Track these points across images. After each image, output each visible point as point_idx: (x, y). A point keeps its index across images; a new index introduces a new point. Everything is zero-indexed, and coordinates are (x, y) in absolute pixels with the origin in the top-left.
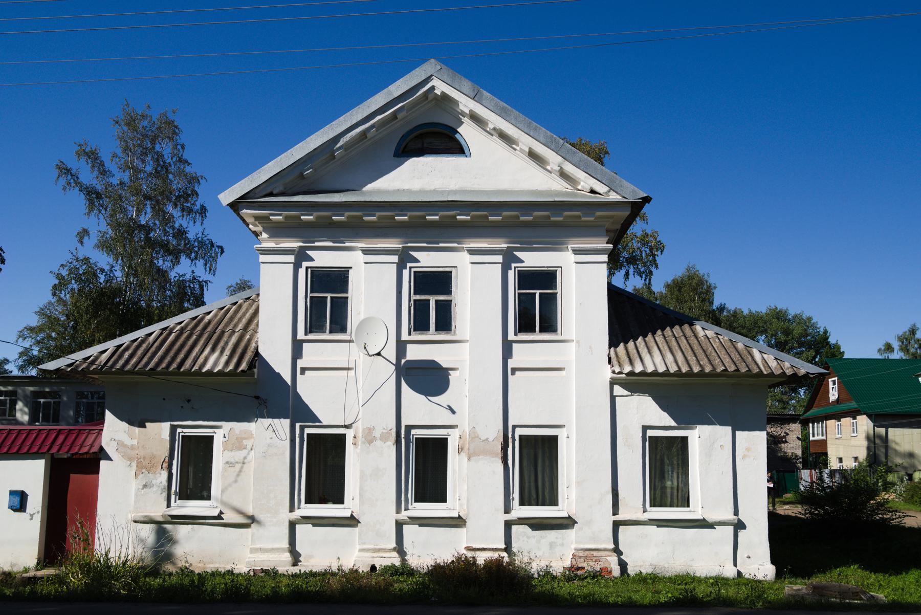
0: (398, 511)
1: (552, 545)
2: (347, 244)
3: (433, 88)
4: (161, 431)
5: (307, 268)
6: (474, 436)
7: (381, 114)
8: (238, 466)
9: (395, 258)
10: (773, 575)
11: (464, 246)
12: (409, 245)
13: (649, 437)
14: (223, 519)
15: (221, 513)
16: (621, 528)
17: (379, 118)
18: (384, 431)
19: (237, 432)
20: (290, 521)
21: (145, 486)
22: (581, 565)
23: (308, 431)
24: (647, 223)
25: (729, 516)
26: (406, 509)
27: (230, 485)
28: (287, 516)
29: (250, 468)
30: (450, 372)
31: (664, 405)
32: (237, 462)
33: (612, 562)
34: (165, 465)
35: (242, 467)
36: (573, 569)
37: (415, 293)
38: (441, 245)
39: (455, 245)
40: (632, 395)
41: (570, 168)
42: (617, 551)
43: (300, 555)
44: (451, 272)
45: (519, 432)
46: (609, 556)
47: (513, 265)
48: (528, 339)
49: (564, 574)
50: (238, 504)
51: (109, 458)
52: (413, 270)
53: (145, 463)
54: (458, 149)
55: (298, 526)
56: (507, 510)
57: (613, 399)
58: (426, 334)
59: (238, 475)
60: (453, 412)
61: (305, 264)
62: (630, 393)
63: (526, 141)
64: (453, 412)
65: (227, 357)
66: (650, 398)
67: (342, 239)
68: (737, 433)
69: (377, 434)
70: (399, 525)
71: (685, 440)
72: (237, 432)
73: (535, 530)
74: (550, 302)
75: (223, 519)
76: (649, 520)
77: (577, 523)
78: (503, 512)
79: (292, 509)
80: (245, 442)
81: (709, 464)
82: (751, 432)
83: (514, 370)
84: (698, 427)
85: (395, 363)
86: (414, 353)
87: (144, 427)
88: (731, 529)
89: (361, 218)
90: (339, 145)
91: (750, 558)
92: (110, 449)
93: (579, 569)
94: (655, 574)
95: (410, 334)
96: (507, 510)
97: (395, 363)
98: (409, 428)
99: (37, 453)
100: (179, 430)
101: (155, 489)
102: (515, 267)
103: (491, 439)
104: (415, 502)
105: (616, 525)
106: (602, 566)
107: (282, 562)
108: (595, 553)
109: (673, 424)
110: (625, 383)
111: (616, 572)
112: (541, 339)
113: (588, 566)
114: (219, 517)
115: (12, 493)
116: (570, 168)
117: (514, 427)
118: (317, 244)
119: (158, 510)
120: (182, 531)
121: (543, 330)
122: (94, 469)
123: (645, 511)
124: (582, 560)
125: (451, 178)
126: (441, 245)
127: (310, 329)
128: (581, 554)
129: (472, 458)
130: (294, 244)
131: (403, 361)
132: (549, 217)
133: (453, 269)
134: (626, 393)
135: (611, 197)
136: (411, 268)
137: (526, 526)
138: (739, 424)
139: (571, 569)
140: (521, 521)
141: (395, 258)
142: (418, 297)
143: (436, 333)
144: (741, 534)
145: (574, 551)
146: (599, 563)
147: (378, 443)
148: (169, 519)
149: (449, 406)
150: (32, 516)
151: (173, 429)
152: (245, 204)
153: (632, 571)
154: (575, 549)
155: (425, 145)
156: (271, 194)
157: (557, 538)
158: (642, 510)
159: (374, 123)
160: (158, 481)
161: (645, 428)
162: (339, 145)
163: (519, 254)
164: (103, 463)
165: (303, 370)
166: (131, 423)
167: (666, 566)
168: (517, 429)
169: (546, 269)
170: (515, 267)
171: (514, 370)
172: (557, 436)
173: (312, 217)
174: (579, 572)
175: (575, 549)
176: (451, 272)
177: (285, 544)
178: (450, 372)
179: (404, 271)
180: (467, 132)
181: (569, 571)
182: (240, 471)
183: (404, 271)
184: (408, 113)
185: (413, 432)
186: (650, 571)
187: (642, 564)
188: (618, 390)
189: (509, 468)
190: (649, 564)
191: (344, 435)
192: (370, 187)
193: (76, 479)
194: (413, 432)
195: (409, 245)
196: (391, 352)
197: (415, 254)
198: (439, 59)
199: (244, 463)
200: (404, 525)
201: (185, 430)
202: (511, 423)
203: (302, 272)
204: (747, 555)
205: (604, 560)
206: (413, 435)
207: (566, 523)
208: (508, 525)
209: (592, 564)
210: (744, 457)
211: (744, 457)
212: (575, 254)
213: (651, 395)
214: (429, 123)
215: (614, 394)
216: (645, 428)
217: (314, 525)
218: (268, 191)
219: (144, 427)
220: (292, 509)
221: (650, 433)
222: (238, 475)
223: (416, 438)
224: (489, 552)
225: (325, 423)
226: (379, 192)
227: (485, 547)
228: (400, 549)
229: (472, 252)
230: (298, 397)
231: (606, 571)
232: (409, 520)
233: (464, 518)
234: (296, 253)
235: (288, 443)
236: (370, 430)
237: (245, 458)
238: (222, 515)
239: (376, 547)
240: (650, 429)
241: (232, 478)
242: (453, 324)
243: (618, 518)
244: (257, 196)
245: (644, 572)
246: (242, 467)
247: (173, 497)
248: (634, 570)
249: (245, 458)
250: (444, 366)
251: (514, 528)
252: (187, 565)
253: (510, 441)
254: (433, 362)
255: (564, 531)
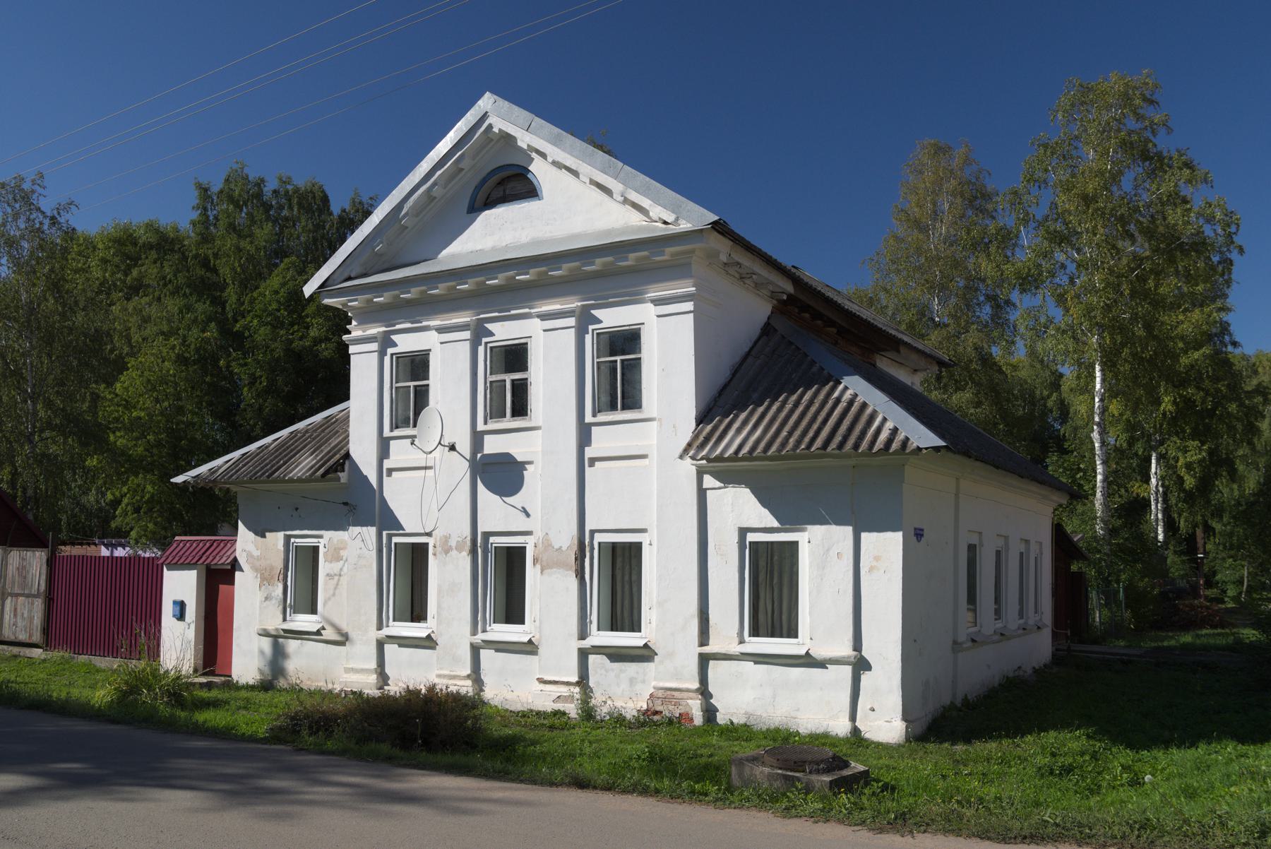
0: (474, 633)
1: (632, 681)
2: (424, 324)
3: (490, 126)
4: (276, 539)
5: (392, 355)
6: (547, 544)
7: (440, 169)
8: (336, 578)
9: (467, 335)
10: (901, 736)
11: (533, 311)
12: (482, 316)
13: (750, 543)
14: (322, 635)
15: (323, 628)
16: (712, 663)
17: (439, 173)
18: (459, 539)
19: (335, 541)
20: (377, 640)
21: (266, 598)
22: (659, 708)
23: (395, 540)
24: (1212, 187)
25: (846, 650)
26: (484, 631)
27: (329, 599)
28: (374, 634)
29: (344, 580)
30: (526, 466)
31: (765, 500)
32: (336, 575)
33: (695, 708)
34: (281, 577)
35: (339, 580)
36: (649, 713)
37: (491, 374)
38: (513, 312)
39: (526, 310)
40: (725, 487)
41: (634, 196)
42: (704, 692)
43: (388, 678)
44: (527, 344)
45: (599, 538)
46: (691, 699)
47: (591, 327)
48: (607, 420)
49: (637, 719)
50: (337, 620)
51: (242, 570)
52: (490, 345)
53: (266, 574)
54: (530, 192)
55: (386, 646)
56: (583, 635)
57: (702, 494)
58: (502, 422)
59: (335, 588)
60: (528, 515)
61: (390, 351)
62: (722, 485)
63: (585, 169)
64: (528, 515)
65: (910, 384)
66: (748, 490)
67: (418, 318)
68: (864, 535)
69: (453, 543)
70: (475, 650)
71: (794, 546)
72: (335, 541)
73: (614, 662)
74: (633, 369)
75: (322, 635)
76: (742, 654)
77: (657, 654)
78: (576, 636)
79: (380, 627)
80: (342, 553)
81: (822, 579)
82: (882, 534)
83: (593, 461)
84: (809, 527)
85: (468, 458)
86: (493, 445)
87: (264, 536)
88: (847, 670)
89: (370, 301)
90: (403, 213)
91: (874, 710)
92: (242, 561)
93: (656, 713)
94: (748, 726)
95: (486, 423)
96: (583, 635)
97: (468, 458)
98: (487, 535)
99: (189, 564)
100: (292, 540)
101: (274, 601)
102: (593, 330)
103: (564, 548)
104: (494, 623)
105: (704, 660)
106: (682, 711)
107: (367, 683)
108: (676, 694)
109: (776, 524)
110: (716, 472)
111: (698, 719)
112: (621, 419)
113: (669, 710)
114: (318, 633)
115: (175, 602)
116: (634, 196)
117: (593, 532)
118: (398, 327)
119: (274, 622)
120: (292, 645)
121: (625, 407)
122: (230, 581)
123: (742, 642)
124: (659, 702)
125: (523, 229)
126: (513, 312)
127: (395, 426)
128: (660, 694)
129: (545, 571)
130: (574, 304)
131: (479, 455)
132: (579, 268)
133: (529, 339)
134: (718, 484)
135: (681, 226)
136: (486, 343)
137: (604, 657)
138: (863, 522)
139: (645, 713)
140: (598, 650)
141: (467, 335)
142: (494, 378)
143: (511, 419)
144: (866, 678)
145: (652, 690)
146: (680, 707)
147: (454, 553)
148: (282, 633)
149: (523, 508)
150: (189, 625)
151: (287, 538)
152: (325, 293)
153: (721, 719)
154: (654, 688)
155: (507, 192)
156: (349, 279)
157: (637, 673)
158: (737, 640)
159: (435, 180)
160: (276, 594)
161: (743, 532)
162: (403, 213)
163: (595, 312)
164: (237, 574)
165: (390, 471)
166: (256, 534)
167: (764, 715)
168: (596, 535)
169: (628, 328)
170: (593, 330)
171: (593, 461)
172: (641, 543)
173: (497, 281)
174: (656, 718)
175: (654, 688)
176: (527, 344)
177: (373, 665)
178: (526, 466)
179: (586, 336)
180: (539, 170)
181: (644, 715)
182: (337, 584)
183: (586, 336)
184: (476, 161)
185: (492, 539)
186: (742, 721)
187: (735, 711)
188: (709, 481)
189: (586, 583)
190: (744, 712)
191: (427, 544)
192: (445, 253)
193: (222, 588)
194: (492, 539)
195: (482, 316)
196: (465, 446)
197: (489, 326)
198: (494, 92)
199: (340, 575)
200: (481, 650)
201: (297, 540)
202: (588, 529)
203: (387, 359)
204: (869, 707)
205: (685, 703)
206: (492, 544)
207: (644, 654)
208: (583, 654)
209: (671, 707)
210: (871, 569)
211: (871, 569)
212: (655, 305)
213: (747, 486)
214: (499, 167)
215: (704, 487)
216: (743, 532)
217: (400, 646)
218: (346, 275)
219: (264, 536)
220: (380, 627)
221: (751, 537)
222: (335, 588)
223: (495, 547)
224: (562, 686)
225: (408, 531)
226: (453, 256)
227: (557, 679)
228: (476, 675)
229: (544, 317)
230: (384, 502)
231: (686, 717)
232: (483, 644)
233: (536, 644)
234: (577, 313)
235: (374, 554)
236: (446, 539)
237: (341, 569)
238: (322, 632)
239: (452, 673)
240: (751, 532)
241: (331, 592)
242: (529, 407)
243: (706, 649)
244: (336, 283)
245: (735, 721)
246: (339, 580)
247: (288, 610)
248: (724, 719)
249: (341, 569)
250: (519, 459)
251: (592, 658)
252: (298, 682)
253: (587, 549)
254: (508, 455)
255: (646, 664)
